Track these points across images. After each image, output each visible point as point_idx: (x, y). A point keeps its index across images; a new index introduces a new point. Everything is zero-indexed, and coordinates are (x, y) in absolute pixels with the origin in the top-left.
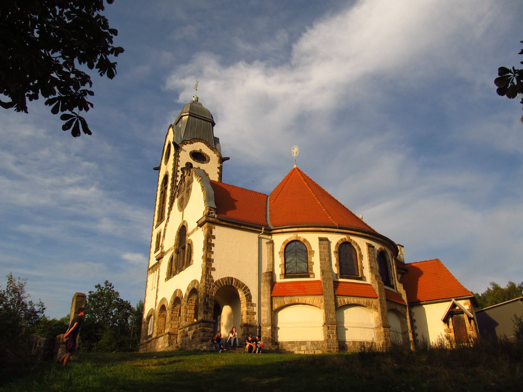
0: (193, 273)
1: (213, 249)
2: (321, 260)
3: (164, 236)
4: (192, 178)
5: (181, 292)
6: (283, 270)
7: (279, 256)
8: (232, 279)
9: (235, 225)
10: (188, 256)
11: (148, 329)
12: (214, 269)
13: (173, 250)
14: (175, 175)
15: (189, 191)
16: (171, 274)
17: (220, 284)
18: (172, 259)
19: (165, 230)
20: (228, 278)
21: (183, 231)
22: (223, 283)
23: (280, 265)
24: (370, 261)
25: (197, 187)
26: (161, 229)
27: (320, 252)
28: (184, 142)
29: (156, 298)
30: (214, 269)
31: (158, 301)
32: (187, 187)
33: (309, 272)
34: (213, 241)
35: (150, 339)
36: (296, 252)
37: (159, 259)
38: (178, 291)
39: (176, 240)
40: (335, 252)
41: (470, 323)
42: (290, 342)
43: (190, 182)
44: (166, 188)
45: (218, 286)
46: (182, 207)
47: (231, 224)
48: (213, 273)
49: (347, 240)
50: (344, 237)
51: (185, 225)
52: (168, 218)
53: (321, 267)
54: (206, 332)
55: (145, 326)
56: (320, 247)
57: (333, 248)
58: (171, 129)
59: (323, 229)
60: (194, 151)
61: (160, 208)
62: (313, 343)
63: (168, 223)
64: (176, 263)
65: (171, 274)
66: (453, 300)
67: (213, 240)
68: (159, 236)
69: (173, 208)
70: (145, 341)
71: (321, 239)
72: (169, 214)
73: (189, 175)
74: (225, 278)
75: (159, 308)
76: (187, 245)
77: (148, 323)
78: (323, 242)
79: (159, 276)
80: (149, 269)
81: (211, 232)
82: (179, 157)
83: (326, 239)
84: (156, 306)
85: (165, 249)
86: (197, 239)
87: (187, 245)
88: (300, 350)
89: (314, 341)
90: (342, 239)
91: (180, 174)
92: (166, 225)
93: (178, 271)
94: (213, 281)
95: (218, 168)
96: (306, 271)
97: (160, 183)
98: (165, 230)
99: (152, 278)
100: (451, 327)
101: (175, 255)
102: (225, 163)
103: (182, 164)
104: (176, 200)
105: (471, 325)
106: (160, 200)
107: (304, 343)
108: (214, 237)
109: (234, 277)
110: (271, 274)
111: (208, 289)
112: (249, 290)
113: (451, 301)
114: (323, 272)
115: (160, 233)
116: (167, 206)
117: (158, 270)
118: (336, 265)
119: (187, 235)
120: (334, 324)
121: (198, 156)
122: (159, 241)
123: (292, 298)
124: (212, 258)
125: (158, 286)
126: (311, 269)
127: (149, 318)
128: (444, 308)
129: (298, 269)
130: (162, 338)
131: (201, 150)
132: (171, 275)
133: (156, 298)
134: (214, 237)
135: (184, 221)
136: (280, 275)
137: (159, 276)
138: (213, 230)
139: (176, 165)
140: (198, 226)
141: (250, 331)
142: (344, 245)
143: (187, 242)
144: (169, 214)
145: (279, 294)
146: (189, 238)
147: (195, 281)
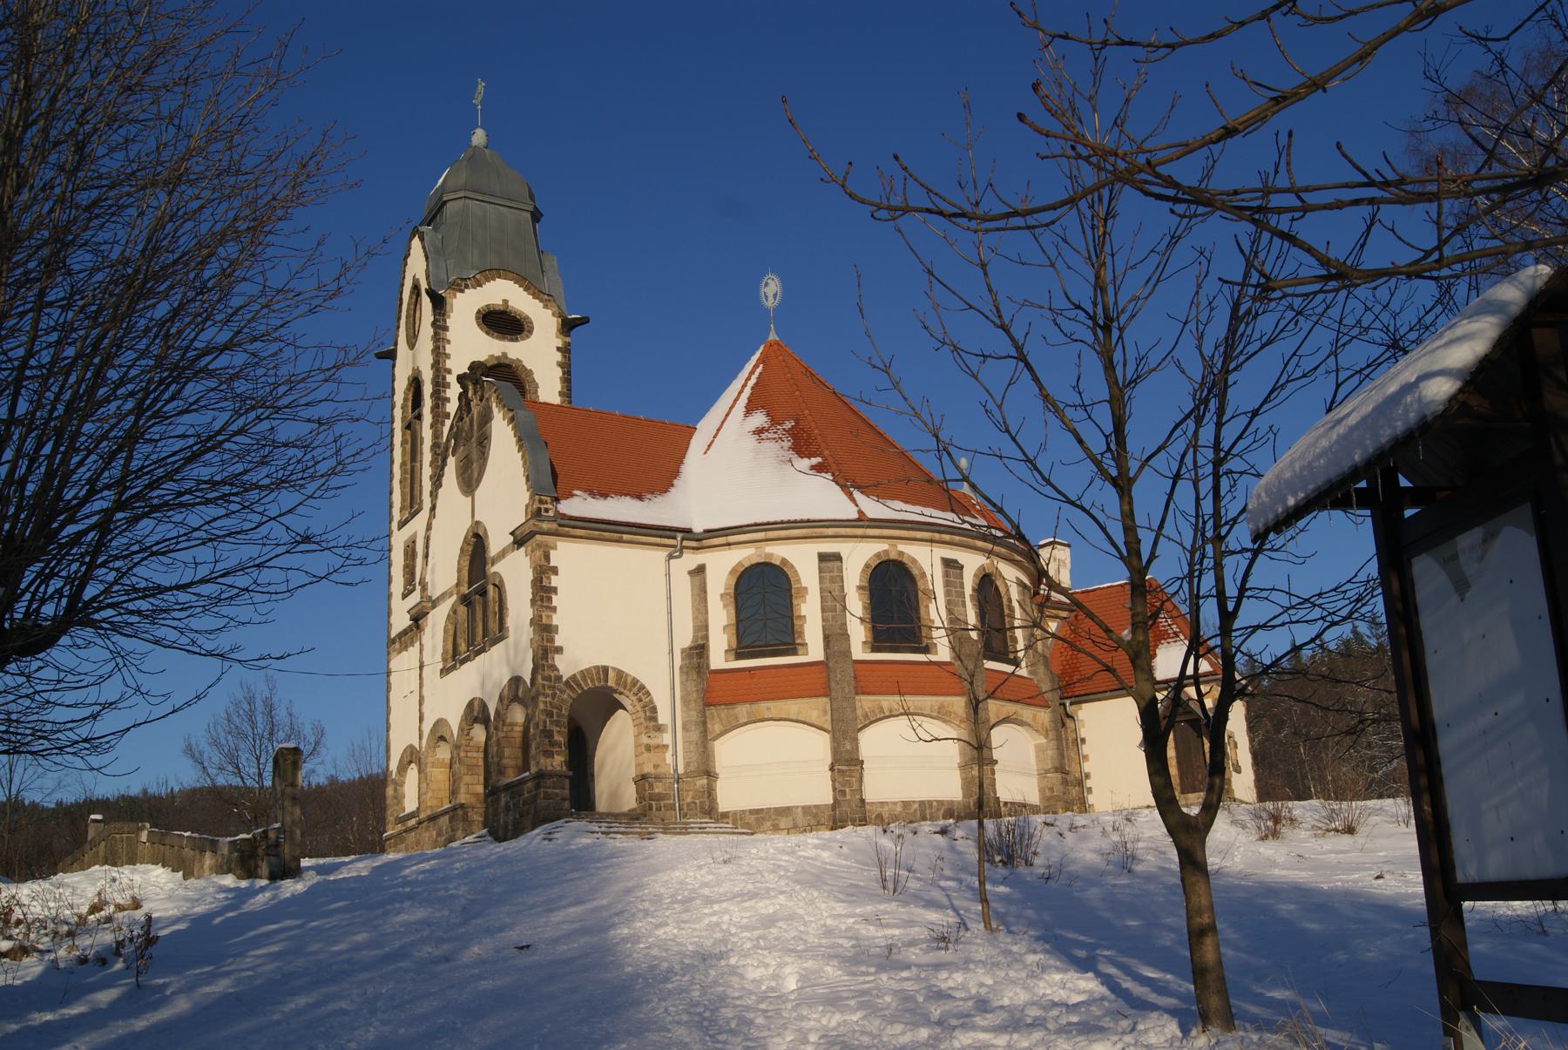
1: (556, 600)
3: (426, 556)
4: (490, 409)
7: (721, 604)
8: (605, 669)
12: (559, 650)
13: (454, 598)
15: (484, 441)
21: (476, 547)
25: (502, 433)
26: (415, 534)
27: (822, 590)
28: (459, 286)
29: (421, 719)
31: (427, 727)
34: (555, 581)
35: (412, 822)
36: (1479, 217)
37: (418, 618)
42: (752, 812)
43: (486, 418)
44: (419, 417)
45: (571, 687)
46: (469, 484)
49: (893, 556)
50: (881, 546)
52: (433, 508)
58: (416, 242)
61: (404, 472)
63: (434, 522)
65: (454, 659)
69: (445, 480)
70: (399, 827)
71: (823, 558)
74: (588, 670)
78: (830, 564)
80: (393, 641)
81: (547, 558)
83: (837, 557)
86: (515, 572)
89: (809, 807)
90: (878, 555)
91: (454, 391)
92: (429, 527)
95: (558, 349)
97: (399, 398)
99: (403, 664)
103: (458, 364)
104: (451, 461)
108: (555, 571)
110: (699, 650)
112: (648, 693)
114: (827, 639)
116: (427, 471)
121: (501, 322)
123: (755, 707)
125: (421, 686)
127: (402, 768)
131: (506, 302)
133: (421, 719)
134: (555, 571)
139: (439, 354)
140: (515, 542)
145: (716, 696)
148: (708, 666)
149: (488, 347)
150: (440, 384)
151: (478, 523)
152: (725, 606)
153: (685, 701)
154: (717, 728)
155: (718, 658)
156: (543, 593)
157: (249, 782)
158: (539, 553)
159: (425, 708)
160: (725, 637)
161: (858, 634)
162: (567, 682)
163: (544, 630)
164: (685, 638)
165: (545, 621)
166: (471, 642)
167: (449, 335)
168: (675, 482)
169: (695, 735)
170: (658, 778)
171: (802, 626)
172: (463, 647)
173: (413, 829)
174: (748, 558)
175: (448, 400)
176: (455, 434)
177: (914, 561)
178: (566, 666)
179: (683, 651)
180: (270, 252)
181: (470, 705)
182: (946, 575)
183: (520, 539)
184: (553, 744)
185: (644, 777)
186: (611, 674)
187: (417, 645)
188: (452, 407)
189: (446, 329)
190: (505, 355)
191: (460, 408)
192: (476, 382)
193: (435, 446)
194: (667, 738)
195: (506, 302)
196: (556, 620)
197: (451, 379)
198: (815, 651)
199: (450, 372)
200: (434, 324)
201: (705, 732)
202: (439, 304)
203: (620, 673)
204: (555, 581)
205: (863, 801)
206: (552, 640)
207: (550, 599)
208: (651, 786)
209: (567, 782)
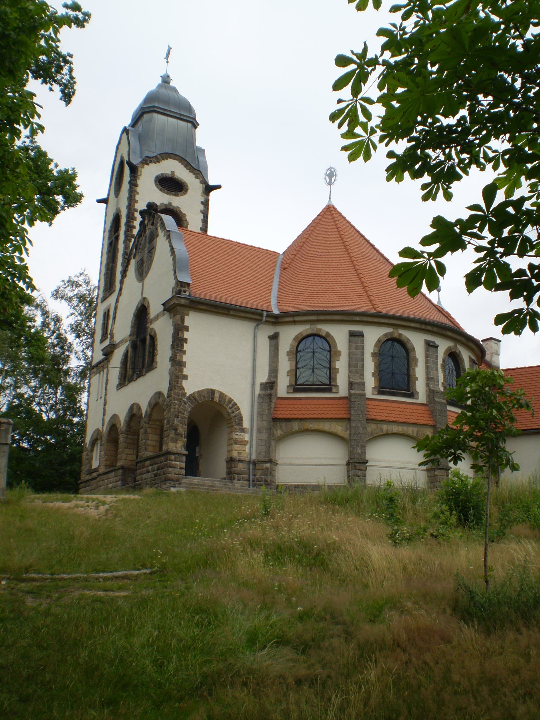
0: (152, 384)
1: (186, 347)
2: (350, 366)
3: (114, 318)
4: (157, 229)
5: (140, 408)
7: (287, 358)
8: (213, 392)
10: (150, 353)
11: (92, 459)
13: (128, 343)
14: (130, 218)
15: (152, 251)
16: (125, 379)
17: (196, 399)
18: (126, 355)
19: (116, 308)
21: (142, 313)
23: (288, 372)
26: (110, 306)
27: (350, 354)
28: (147, 161)
29: (104, 415)
30: (185, 377)
33: (333, 383)
34: (186, 335)
35: (95, 475)
38: (135, 406)
39: (132, 327)
44: (117, 238)
48: (184, 383)
50: (388, 330)
52: (121, 289)
55: (87, 455)
56: (350, 347)
60: (162, 174)
63: (121, 298)
64: (134, 363)
65: (125, 379)
67: (185, 333)
68: (106, 316)
72: (122, 282)
73: (153, 224)
74: (202, 391)
75: (108, 428)
77: (92, 451)
79: (107, 380)
84: (103, 425)
86: (162, 328)
89: (331, 486)
90: (386, 335)
92: (117, 301)
93: (135, 376)
95: (202, 203)
96: (328, 382)
98: (116, 308)
102: (213, 194)
103: (141, 205)
104: (133, 262)
111: (177, 407)
112: (238, 409)
114: (351, 385)
115: (109, 310)
116: (119, 268)
117: (105, 370)
118: (374, 354)
119: (149, 321)
122: (107, 324)
124: (184, 360)
125: (106, 395)
127: (94, 442)
129: (315, 379)
131: (173, 172)
132: (125, 380)
133: (104, 415)
134: (187, 329)
136: (288, 386)
137: (107, 380)
138: (186, 318)
139: (132, 200)
142: (390, 342)
143: (149, 331)
144: (122, 282)
146: (151, 326)
148: (276, 394)
149: (161, 198)
150: (130, 218)
151: (144, 299)
153: (260, 414)
156: (178, 342)
159: (107, 408)
160: (288, 378)
161: (370, 382)
162: (189, 397)
163: (177, 364)
164: (263, 377)
166: (134, 369)
168: (183, 166)
169: (265, 436)
172: (130, 372)
173: (95, 478)
175: (134, 227)
176: (136, 246)
177: (408, 340)
178: (190, 387)
179: (261, 384)
180: (345, 409)
182: (427, 351)
184: (177, 434)
186: (217, 395)
189: (136, 185)
190: (170, 204)
191: (139, 231)
192: (150, 214)
193: (125, 253)
194: (247, 437)
195: (173, 172)
196: (185, 358)
197: (137, 215)
199: (136, 211)
200: (130, 183)
202: (134, 170)
203: (222, 395)
204: (186, 335)
206: (181, 371)
207: (182, 346)
209: (184, 459)
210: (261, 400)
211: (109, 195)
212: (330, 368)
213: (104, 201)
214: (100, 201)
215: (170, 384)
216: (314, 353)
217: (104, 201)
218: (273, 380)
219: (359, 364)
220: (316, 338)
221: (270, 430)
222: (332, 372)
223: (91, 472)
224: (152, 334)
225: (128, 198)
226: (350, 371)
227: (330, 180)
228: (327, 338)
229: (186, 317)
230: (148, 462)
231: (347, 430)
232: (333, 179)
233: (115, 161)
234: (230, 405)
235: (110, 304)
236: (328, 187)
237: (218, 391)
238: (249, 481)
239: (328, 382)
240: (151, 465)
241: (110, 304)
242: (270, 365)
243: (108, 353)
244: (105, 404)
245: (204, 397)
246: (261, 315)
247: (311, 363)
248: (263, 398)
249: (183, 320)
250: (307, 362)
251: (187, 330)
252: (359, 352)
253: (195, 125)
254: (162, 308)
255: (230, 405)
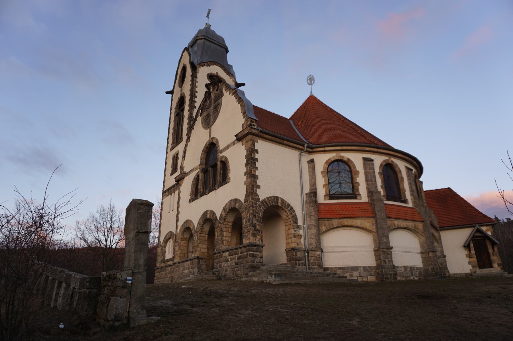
1: (257, 164)
3: (184, 157)
5: (214, 213)
6: (328, 191)
7: (321, 176)
8: (277, 198)
9: (278, 140)
11: (165, 252)
12: (259, 187)
16: (196, 194)
18: (197, 179)
19: (185, 151)
20: (274, 197)
22: (269, 202)
23: (324, 186)
24: (410, 183)
28: (202, 64)
29: (177, 221)
30: (259, 187)
31: (180, 224)
32: (215, 103)
38: (209, 213)
39: (201, 159)
40: (379, 173)
41: (493, 248)
42: (340, 268)
44: (183, 111)
46: (208, 124)
47: (273, 138)
48: (258, 191)
49: (390, 162)
50: (385, 158)
51: (214, 142)
53: (368, 188)
54: (256, 257)
55: (162, 249)
57: (377, 169)
59: (368, 149)
62: (365, 268)
65: (196, 194)
66: (477, 226)
70: (163, 265)
71: (365, 160)
74: (270, 197)
76: (219, 163)
77: (165, 247)
78: (369, 162)
82: (196, 77)
85: (186, 170)
87: (219, 163)
88: (351, 276)
89: (366, 267)
90: (385, 161)
94: (259, 199)
98: (185, 151)
100: (473, 252)
101: (201, 175)
105: (494, 251)
106: (175, 124)
107: (355, 269)
109: (279, 195)
110: (313, 194)
111: (254, 209)
112: (294, 211)
113: (474, 227)
115: (177, 154)
116: (185, 127)
118: (382, 187)
120: (383, 250)
123: (341, 220)
124: (257, 174)
126: (358, 190)
127: (166, 241)
128: (463, 235)
130: (189, 262)
131: (217, 73)
133: (177, 221)
134: (257, 152)
135: (213, 138)
136: (325, 196)
140: (237, 140)
141: (298, 256)
145: (325, 217)
147: (236, 200)
152: (323, 177)
154: (324, 228)
155: (321, 198)
156: (251, 160)
157: (102, 245)
158: (250, 143)
159: (179, 216)
162: (262, 202)
163: (252, 176)
164: (307, 189)
165: (253, 172)
167: (197, 80)
169: (314, 231)
170: (299, 250)
171: (358, 187)
173: (170, 266)
174: (333, 157)
177: (397, 165)
178: (263, 194)
181: (205, 213)
183: (239, 138)
185: (293, 249)
186: (280, 201)
187: (177, 192)
188: (197, 105)
194: (301, 232)
195: (217, 73)
196: (257, 173)
198: (364, 197)
201: (319, 230)
202: (194, 68)
203: (283, 201)
205: (394, 265)
206: (256, 182)
207: (255, 164)
208: (296, 254)
210: (308, 205)
211: (174, 88)
212: (352, 183)
213: (171, 93)
214: (167, 93)
215: (247, 192)
216: (339, 172)
217: (171, 93)
218: (313, 191)
219: (373, 179)
220: (340, 163)
221: (318, 226)
222: (354, 186)
223: (164, 261)
224: (224, 159)
225: (191, 85)
226: (367, 184)
227: (311, 82)
228: (347, 163)
229: (256, 143)
230: (227, 253)
231: (373, 225)
232: (312, 82)
233: (178, 68)
234: (289, 209)
235: (178, 151)
236: (310, 86)
237: (281, 198)
238: (306, 265)
239: (351, 192)
240: (229, 255)
241: (178, 151)
242: (310, 181)
243: (179, 181)
244: (178, 214)
245: (272, 202)
246: (303, 146)
247: (338, 179)
248: (310, 203)
249: (254, 146)
250: (335, 179)
251: (258, 153)
252: (372, 171)
253: (227, 51)
254: (235, 138)
255: (289, 209)
